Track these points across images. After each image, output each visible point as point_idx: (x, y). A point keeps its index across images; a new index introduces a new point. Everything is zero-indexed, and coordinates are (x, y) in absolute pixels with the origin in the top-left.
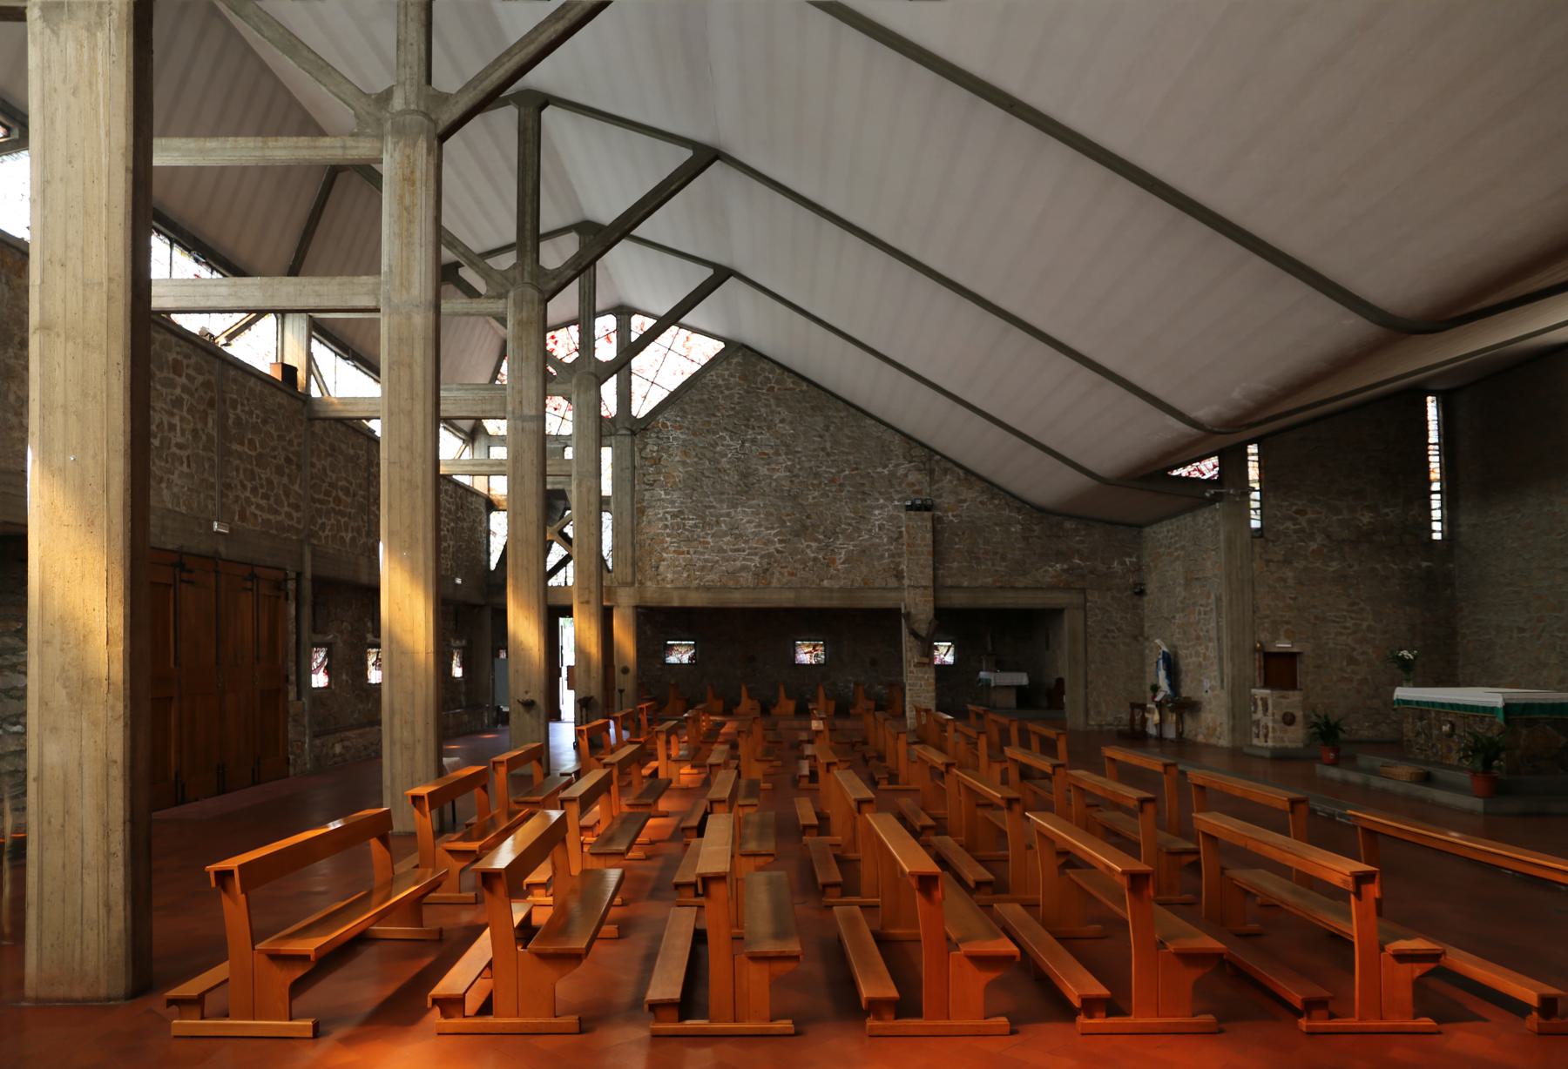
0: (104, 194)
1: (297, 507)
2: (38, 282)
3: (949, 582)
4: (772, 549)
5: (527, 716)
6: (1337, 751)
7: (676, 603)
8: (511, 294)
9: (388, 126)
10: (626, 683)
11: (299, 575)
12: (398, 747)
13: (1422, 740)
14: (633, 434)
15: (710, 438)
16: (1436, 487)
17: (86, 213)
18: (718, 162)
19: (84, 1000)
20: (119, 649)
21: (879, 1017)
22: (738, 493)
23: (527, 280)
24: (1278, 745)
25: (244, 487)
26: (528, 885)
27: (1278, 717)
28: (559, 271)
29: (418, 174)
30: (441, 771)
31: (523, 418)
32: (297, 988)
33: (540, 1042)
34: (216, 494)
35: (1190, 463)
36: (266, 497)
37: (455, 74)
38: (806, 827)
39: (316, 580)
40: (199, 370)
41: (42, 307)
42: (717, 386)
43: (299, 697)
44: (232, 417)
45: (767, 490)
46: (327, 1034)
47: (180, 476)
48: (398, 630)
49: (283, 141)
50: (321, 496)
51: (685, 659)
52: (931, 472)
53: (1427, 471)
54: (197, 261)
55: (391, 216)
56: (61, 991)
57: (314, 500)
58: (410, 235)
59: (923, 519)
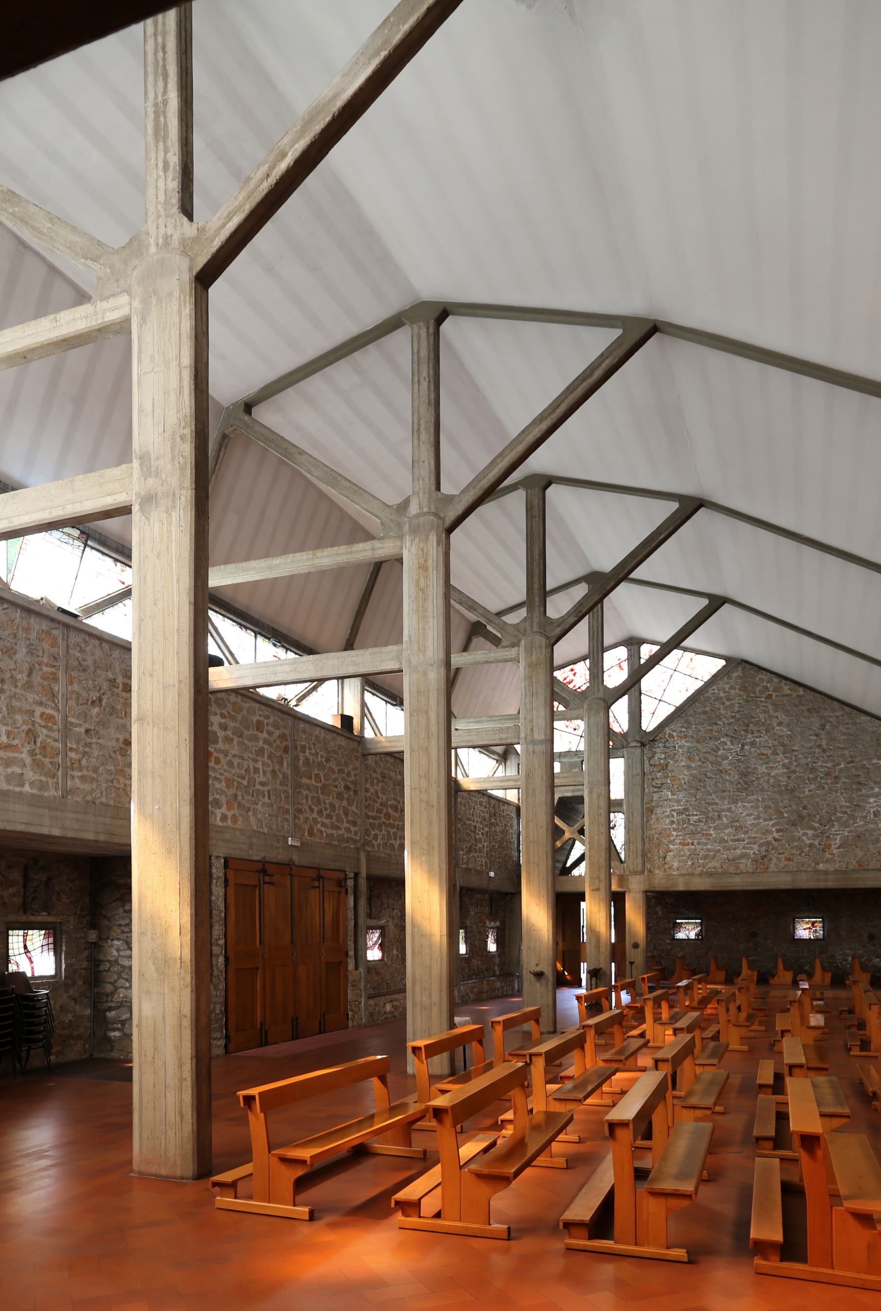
1: (354, 824)
2: (136, 689)
4: (770, 838)
5: (538, 984)
7: (681, 888)
8: (523, 643)
9: (406, 527)
10: (636, 956)
11: (356, 875)
12: (419, 1007)
14: (643, 745)
15: (712, 744)
17: (165, 638)
18: (702, 510)
19: (167, 1177)
20: (188, 938)
21: (765, 1257)
22: (738, 790)
23: (536, 629)
25: (312, 810)
26: (502, 1121)
28: (563, 619)
29: (430, 562)
30: (452, 1026)
31: (534, 742)
32: (301, 1185)
33: (476, 1243)
34: (290, 817)
36: (329, 817)
37: (459, 478)
38: (761, 1086)
39: (370, 878)
40: (276, 726)
41: (139, 705)
42: (718, 699)
43: (356, 968)
44: (302, 758)
45: (766, 786)
46: (319, 1219)
47: (263, 806)
48: (418, 918)
49: (328, 551)
50: (374, 814)
51: (692, 935)
54: (275, 645)
56: (153, 1169)
57: (368, 817)
58: (425, 610)
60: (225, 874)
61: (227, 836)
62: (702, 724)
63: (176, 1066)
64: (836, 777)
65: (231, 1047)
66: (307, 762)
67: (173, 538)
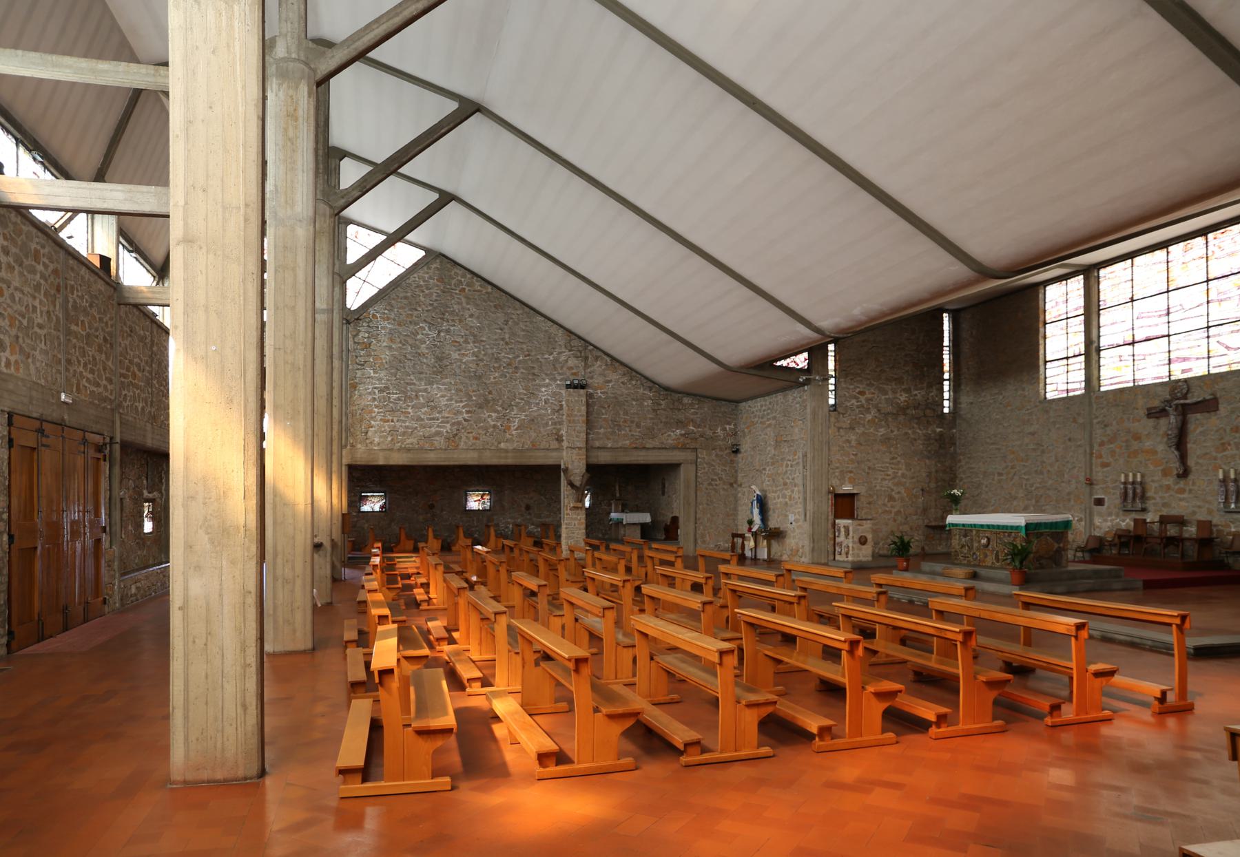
0: (241, 136)
3: (597, 444)
4: (460, 418)
6: (907, 560)
7: (381, 462)
13: (965, 550)
16: (946, 376)
19: (225, 780)
22: (434, 373)
24: (856, 559)
27: (856, 539)
29: (300, 112)
34: (62, 369)
35: (789, 356)
36: (92, 372)
42: (418, 286)
48: (281, 486)
50: (124, 371)
51: (377, 508)
52: (587, 358)
53: (942, 365)
55: (276, 145)
56: (205, 775)
59: (580, 395)
60: (9, 433)
61: (11, 386)
62: (403, 308)
63: (238, 651)
64: (516, 368)
65: (14, 645)
66: (75, 307)
67: (237, 36)
